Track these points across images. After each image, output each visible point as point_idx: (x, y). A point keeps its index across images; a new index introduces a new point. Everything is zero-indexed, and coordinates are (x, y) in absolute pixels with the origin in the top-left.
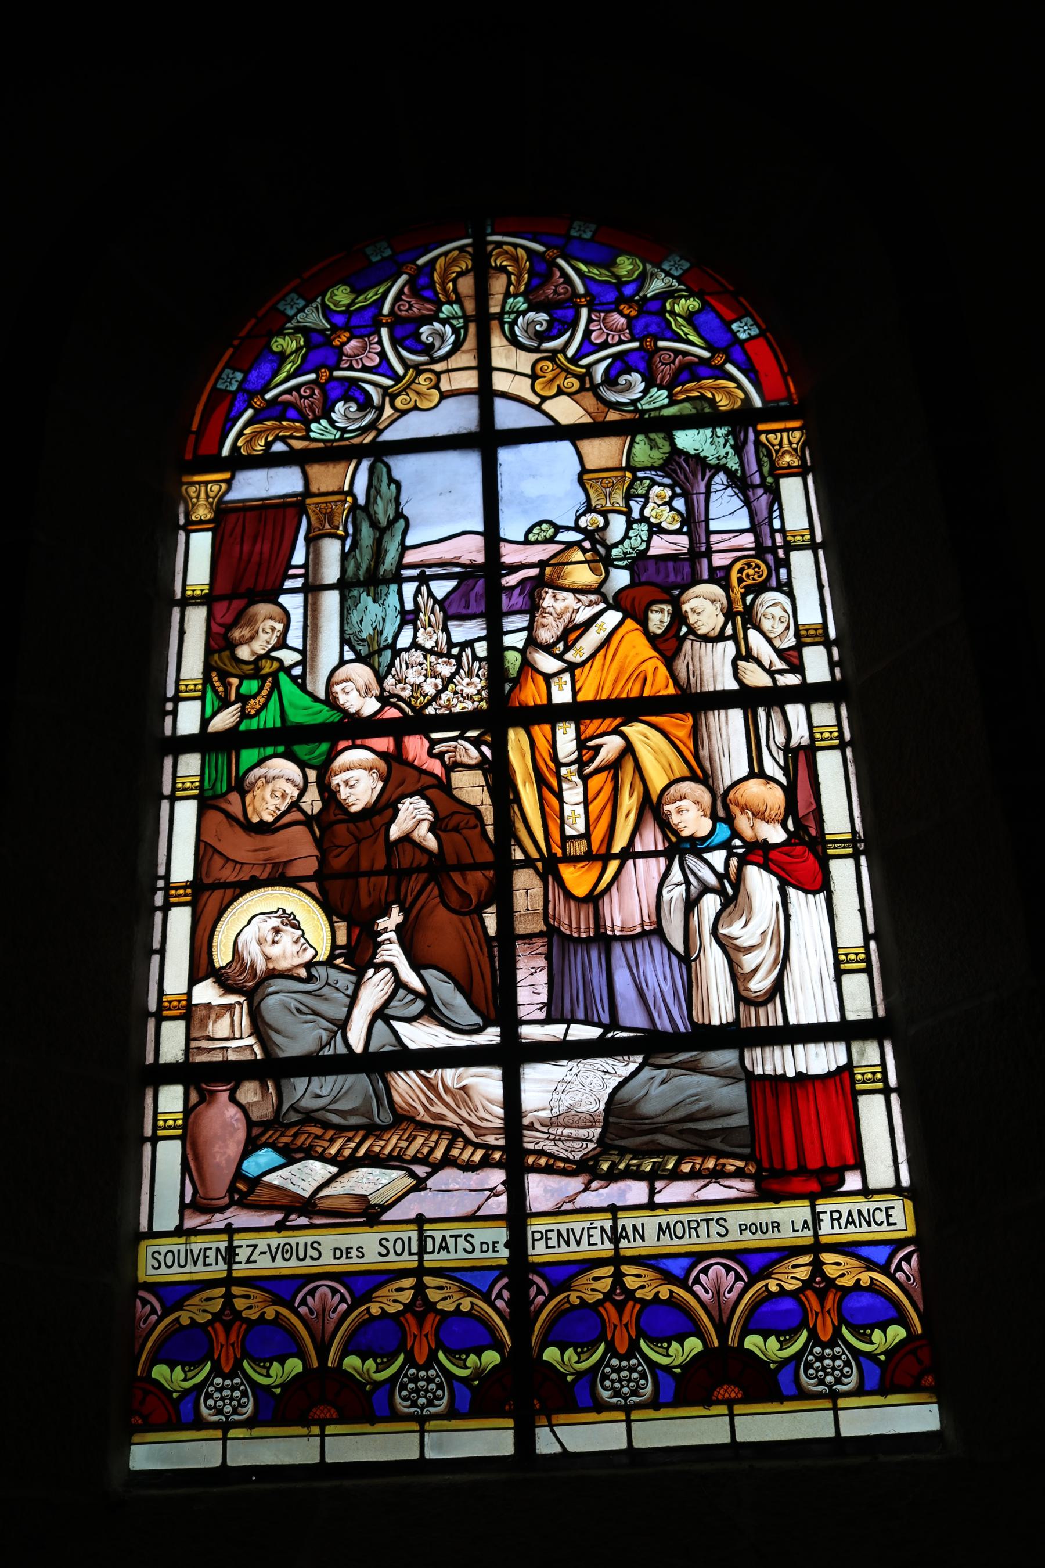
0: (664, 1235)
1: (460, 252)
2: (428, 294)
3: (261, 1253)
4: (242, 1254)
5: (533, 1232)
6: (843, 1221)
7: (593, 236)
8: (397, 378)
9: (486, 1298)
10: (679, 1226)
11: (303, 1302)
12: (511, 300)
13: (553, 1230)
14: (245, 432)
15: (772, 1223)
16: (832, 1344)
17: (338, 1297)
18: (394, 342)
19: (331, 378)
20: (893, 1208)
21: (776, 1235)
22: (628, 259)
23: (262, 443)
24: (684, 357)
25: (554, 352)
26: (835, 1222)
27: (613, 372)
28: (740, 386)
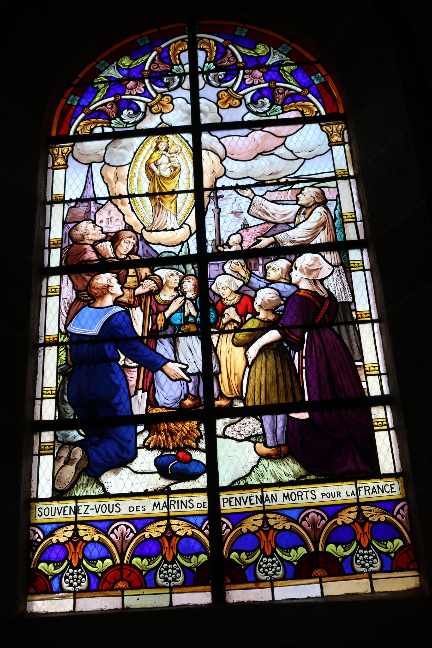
0: (286, 499)
1: (182, 42)
2: (167, 61)
3: (91, 509)
4: (82, 510)
5: (223, 499)
6: (371, 491)
7: (246, 35)
8: (153, 99)
9: (200, 529)
10: (293, 495)
11: (113, 532)
12: (207, 64)
13: (233, 498)
14: (80, 124)
15: (337, 492)
16: (172, 562)
17: (129, 530)
18: (150, 83)
19: (121, 99)
20: (394, 484)
21: (339, 498)
22: (263, 46)
23: (89, 129)
24: (289, 91)
25: (228, 88)
26: (367, 492)
27: (256, 97)
28: (315, 106)
